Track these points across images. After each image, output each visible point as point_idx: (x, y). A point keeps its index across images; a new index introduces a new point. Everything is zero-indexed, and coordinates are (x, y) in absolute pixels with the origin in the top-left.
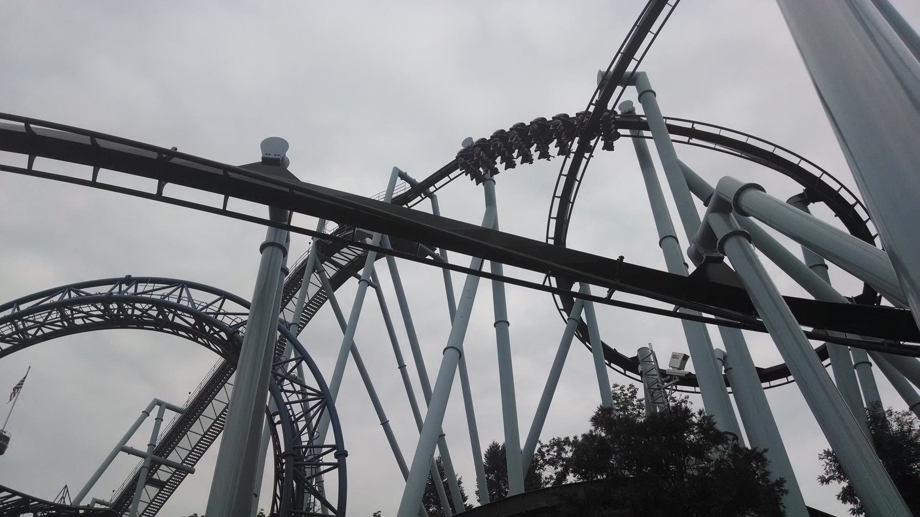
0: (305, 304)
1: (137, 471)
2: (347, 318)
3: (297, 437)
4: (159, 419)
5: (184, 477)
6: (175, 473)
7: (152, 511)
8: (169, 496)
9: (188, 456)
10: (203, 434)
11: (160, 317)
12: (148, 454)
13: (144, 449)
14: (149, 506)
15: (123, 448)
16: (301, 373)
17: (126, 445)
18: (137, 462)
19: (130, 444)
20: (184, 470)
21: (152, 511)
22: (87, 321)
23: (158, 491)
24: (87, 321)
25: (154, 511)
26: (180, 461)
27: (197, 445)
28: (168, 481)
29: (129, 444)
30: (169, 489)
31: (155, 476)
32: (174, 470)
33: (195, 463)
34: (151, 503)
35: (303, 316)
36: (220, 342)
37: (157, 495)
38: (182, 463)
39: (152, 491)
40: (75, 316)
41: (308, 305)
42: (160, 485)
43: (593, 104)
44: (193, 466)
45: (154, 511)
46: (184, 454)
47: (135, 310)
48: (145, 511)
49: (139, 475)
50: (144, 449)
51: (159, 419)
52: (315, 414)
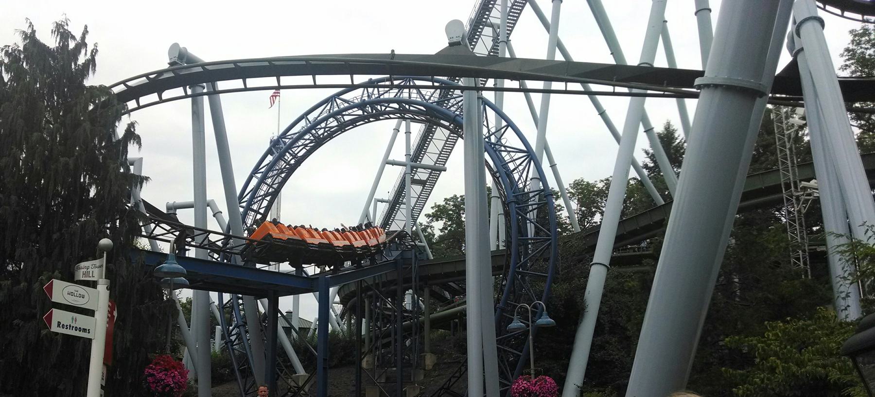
0: (508, 9)
1: (402, 176)
2: (549, 17)
3: (515, 186)
4: (408, 133)
5: (439, 174)
6: (431, 173)
7: (428, 189)
8: (431, 190)
9: (438, 158)
10: (446, 139)
11: (365, 114)
12: (408, 163)
13: (403, 159)
14: (418, 200)
15: (387, 162)
16: (498, 123)
17: (389, 159)
18: (399, 171)
19: (391, 158)
20: (437, 170)
21: (428, 189)
22: (307, 148)
23: (422, 187)
24: (307, 148)
25: (449, 149)
26: (433, 164)
27: (443, 148)
28: (428, 179)
29: (391, 158)
30: (430, 185)
31: (416, 177)
32: (430, 171)
33: (445, 162)
34: (419, 197)
35: (508, 23)
36: (419, 113)
37: (422, 191)
38: (435, 164)
39: (418, 188)
40: (296, 152)
41: (512, 8)
42: (422, 183)
43: (825, 7)
44: (444, 165)
45: (449, 149)
46: (435, 157)
47: (345, 117)
48: (416, 204)
49: (405, 178)
50: (403, 159)
51: (408, 133)
52: (524, 169)
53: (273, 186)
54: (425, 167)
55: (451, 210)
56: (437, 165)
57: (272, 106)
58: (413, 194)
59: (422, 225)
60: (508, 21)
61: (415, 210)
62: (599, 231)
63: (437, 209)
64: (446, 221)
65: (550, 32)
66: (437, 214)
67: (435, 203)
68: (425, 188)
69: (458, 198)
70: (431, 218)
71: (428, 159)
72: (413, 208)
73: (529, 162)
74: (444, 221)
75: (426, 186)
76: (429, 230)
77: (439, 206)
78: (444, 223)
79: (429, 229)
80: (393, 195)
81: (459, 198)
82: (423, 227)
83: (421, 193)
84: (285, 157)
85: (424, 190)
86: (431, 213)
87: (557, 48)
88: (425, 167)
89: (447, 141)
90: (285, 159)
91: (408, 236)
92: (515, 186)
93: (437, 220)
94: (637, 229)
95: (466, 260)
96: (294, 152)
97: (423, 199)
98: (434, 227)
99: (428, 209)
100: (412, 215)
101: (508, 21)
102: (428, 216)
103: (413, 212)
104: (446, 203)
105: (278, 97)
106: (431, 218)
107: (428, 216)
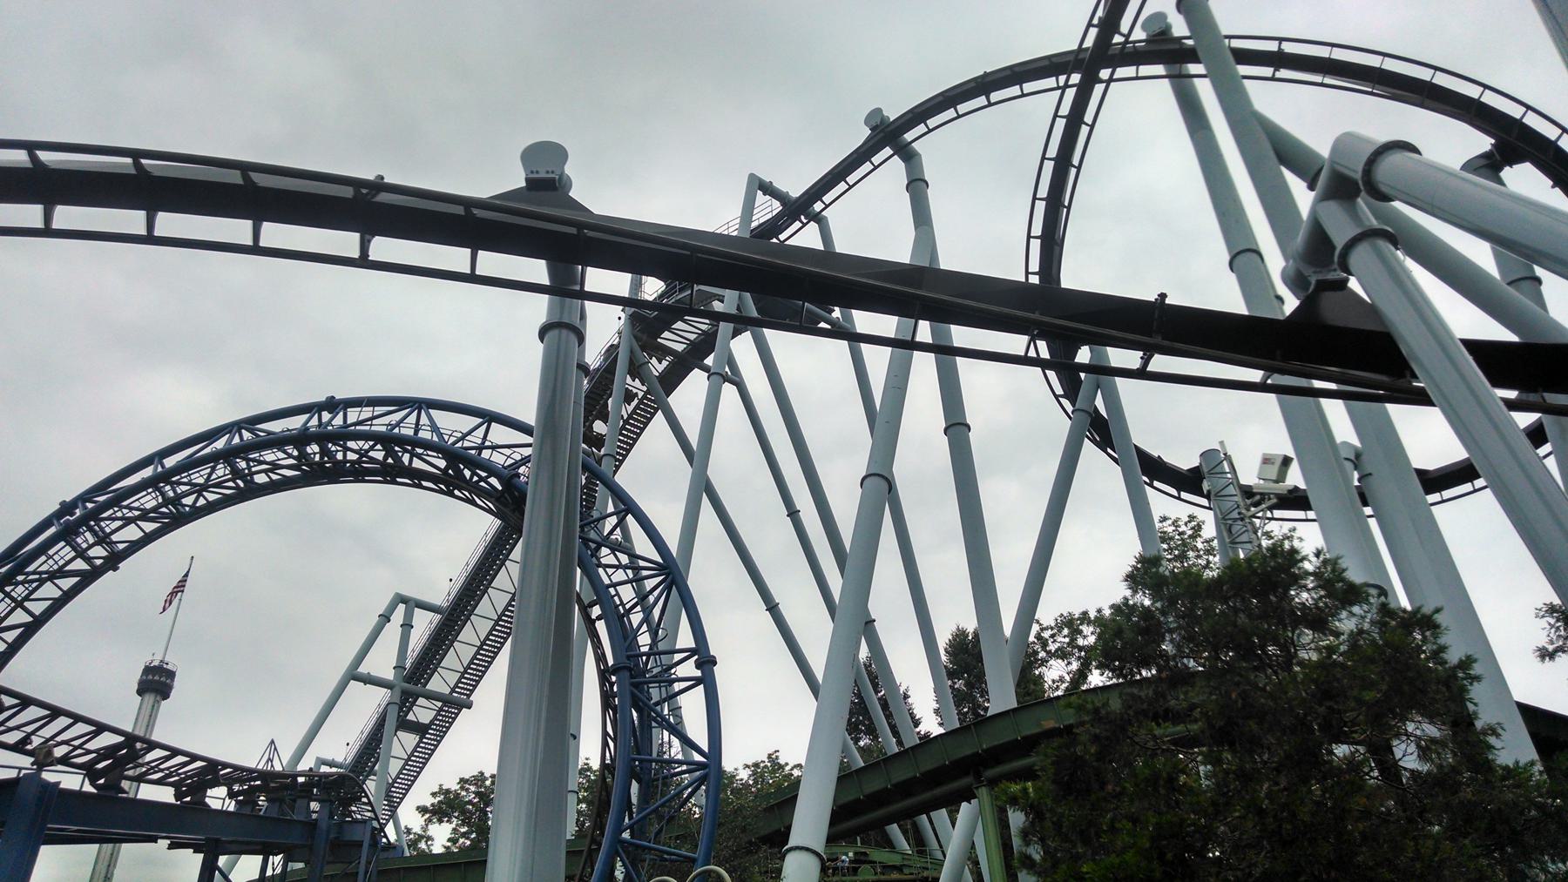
1: (381, 710)
3: (630, 638)
4: (407, 626)
5: (457, 715)
6: (441, 709)
9: (459, 681)
10: (479, 644)
13: (389, 674)
18: (376, 698)
20: (454, 704)
26: (447, 691)
28: (432, 722)
29: (363, 669)
31: (411, 717)
32: (439, 704)
33: (472, 691)
35: (619, 447)
37: (418, 746)
38: (451, 693)
39: (409, 740)
42: (420, 729)
44: (469, 696)
46: (453, 678)
48: (400, 772)
50: (389, 674)
51: (407, 626)
53: (26, 604)
54: (431, 696)
55: (470, 802)
56: (454, 694)
57: (164, 610)
58: (396, 750)
59: (410, 833)
60: (619, 444)
61: (396, 785)
62: (797, 795)
63: (442, 797)
64: (457, 825)
65: (694, 464)
66: (440, 808)
67: (440, 785)
68: (424, 740)
69: (486, 779)
70: (427, 816)
71: (439, 683)
72: (394, 781)
73: (669, 588)
74: (453, 826)
75: (430, 731)
76: (423, 845)
77: (448, 791)
78: (454, 829)
79: (423, 842)
80: (355, 751)
81: (487, 779)
82: (412, 836)
83: (415, 750)
84: (79, 540)
85: (422, 745)
86: (428, 805)
87: (704, 494)
88: (431, 696)
89: (480, 648)
90: (76, 543)
91: (365, 800)
92: (630, 638)
93: (440, 821)
94: (887, 787)
95: (489, 865)
96: (102, 529)
97: (416, 764)
98: (433, 840)
99: (422, 793)
100: (387, 796)
101: (619, 444)
102: (422, 810)
103: (393, 789)
104: (462, 788)
105: (179, 594)
106: (427, 816)
107: (422, 810)
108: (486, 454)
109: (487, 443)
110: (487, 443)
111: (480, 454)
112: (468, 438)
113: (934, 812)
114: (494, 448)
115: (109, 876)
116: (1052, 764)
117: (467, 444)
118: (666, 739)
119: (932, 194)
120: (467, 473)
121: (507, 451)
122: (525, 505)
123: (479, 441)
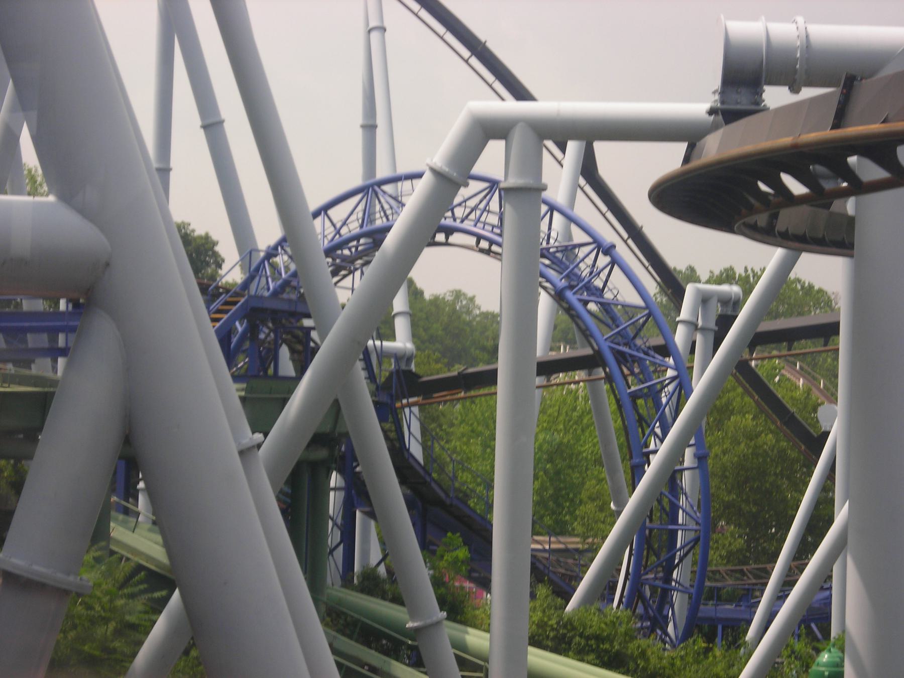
108: (344, 231)
109: (338, 226)
110: (338, 226)
111: (340, 236)
112: (326, 233)
113: (343, 496)
114: (344, 223)
115: (583, 327)
116: (627, 609)
117: (330, 237)
118: (698, 514)
119: (358, 118)
120: (346, 252)
121: (353, 217)
122: (813, 555)
123: (332, 229)
